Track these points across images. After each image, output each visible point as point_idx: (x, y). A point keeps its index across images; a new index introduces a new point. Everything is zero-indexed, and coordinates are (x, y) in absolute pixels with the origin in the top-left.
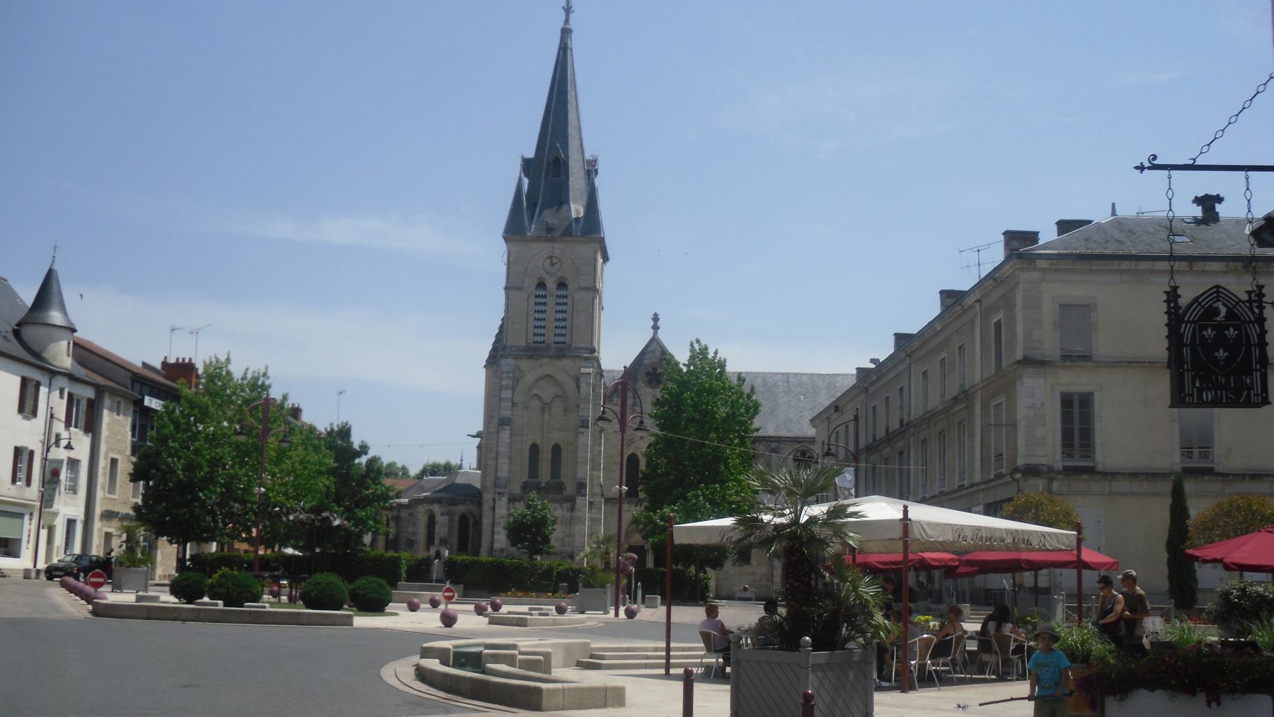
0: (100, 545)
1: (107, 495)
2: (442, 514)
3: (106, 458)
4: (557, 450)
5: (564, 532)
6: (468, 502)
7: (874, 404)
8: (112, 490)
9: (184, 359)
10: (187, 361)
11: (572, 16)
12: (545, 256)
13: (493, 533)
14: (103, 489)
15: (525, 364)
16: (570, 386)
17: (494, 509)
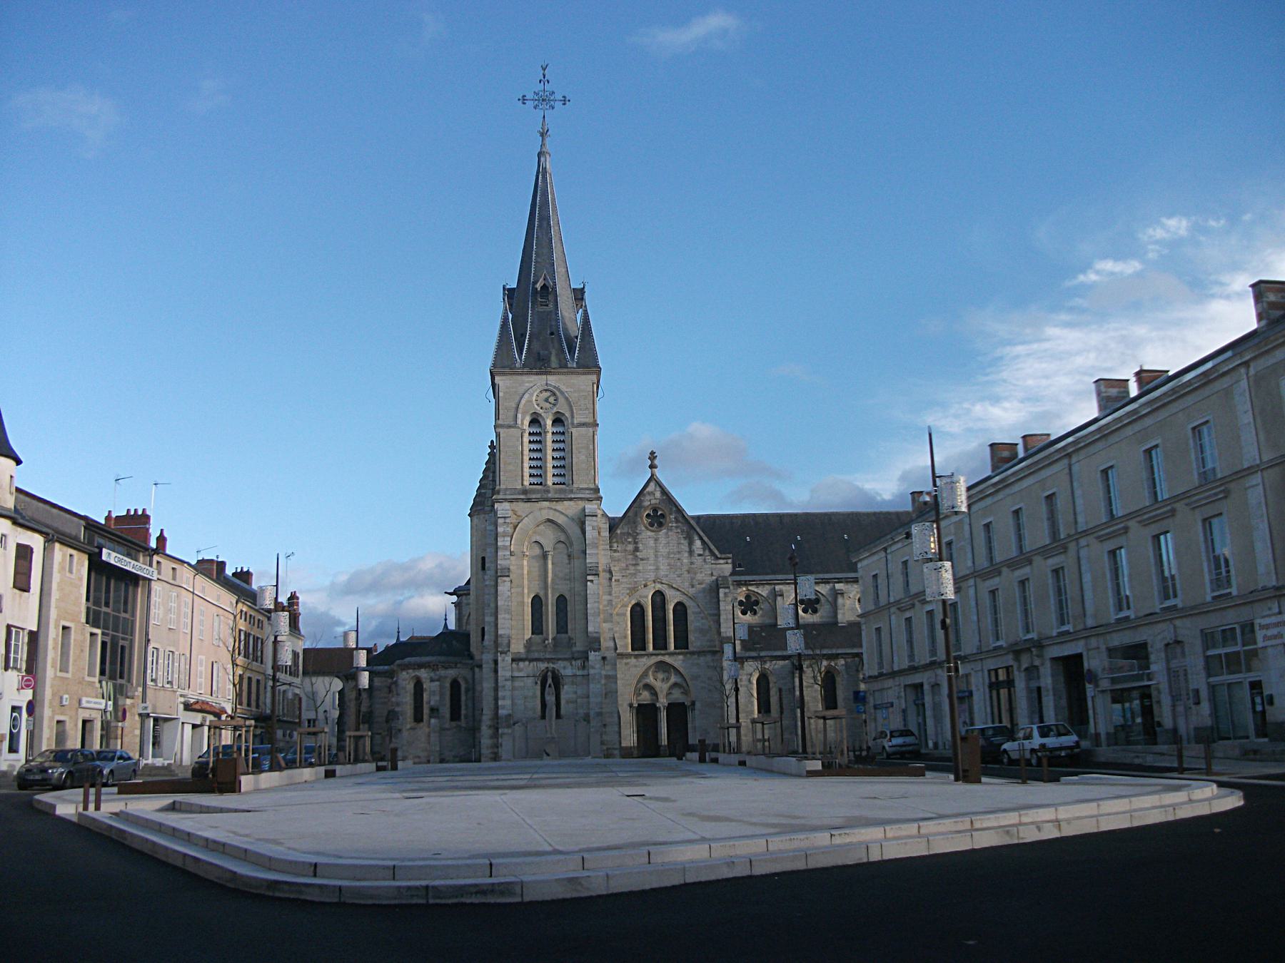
0: (51, 736)
1: (59, 674)
2: (432, 680)
3: (56, 627)
4: (561, 601)
5: (576, 693)
6: (459, 665)
7: (989, 520)
8: (64, 669)
9: (136, 511)
10: (140, 512)
11: (547, 140)
12: (539, 391)
13: (496, 699)
14: (54, 666)
15: (522, 507)
16: (574, 531)
17: (496, 671)
